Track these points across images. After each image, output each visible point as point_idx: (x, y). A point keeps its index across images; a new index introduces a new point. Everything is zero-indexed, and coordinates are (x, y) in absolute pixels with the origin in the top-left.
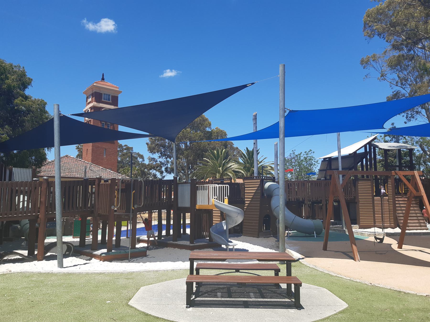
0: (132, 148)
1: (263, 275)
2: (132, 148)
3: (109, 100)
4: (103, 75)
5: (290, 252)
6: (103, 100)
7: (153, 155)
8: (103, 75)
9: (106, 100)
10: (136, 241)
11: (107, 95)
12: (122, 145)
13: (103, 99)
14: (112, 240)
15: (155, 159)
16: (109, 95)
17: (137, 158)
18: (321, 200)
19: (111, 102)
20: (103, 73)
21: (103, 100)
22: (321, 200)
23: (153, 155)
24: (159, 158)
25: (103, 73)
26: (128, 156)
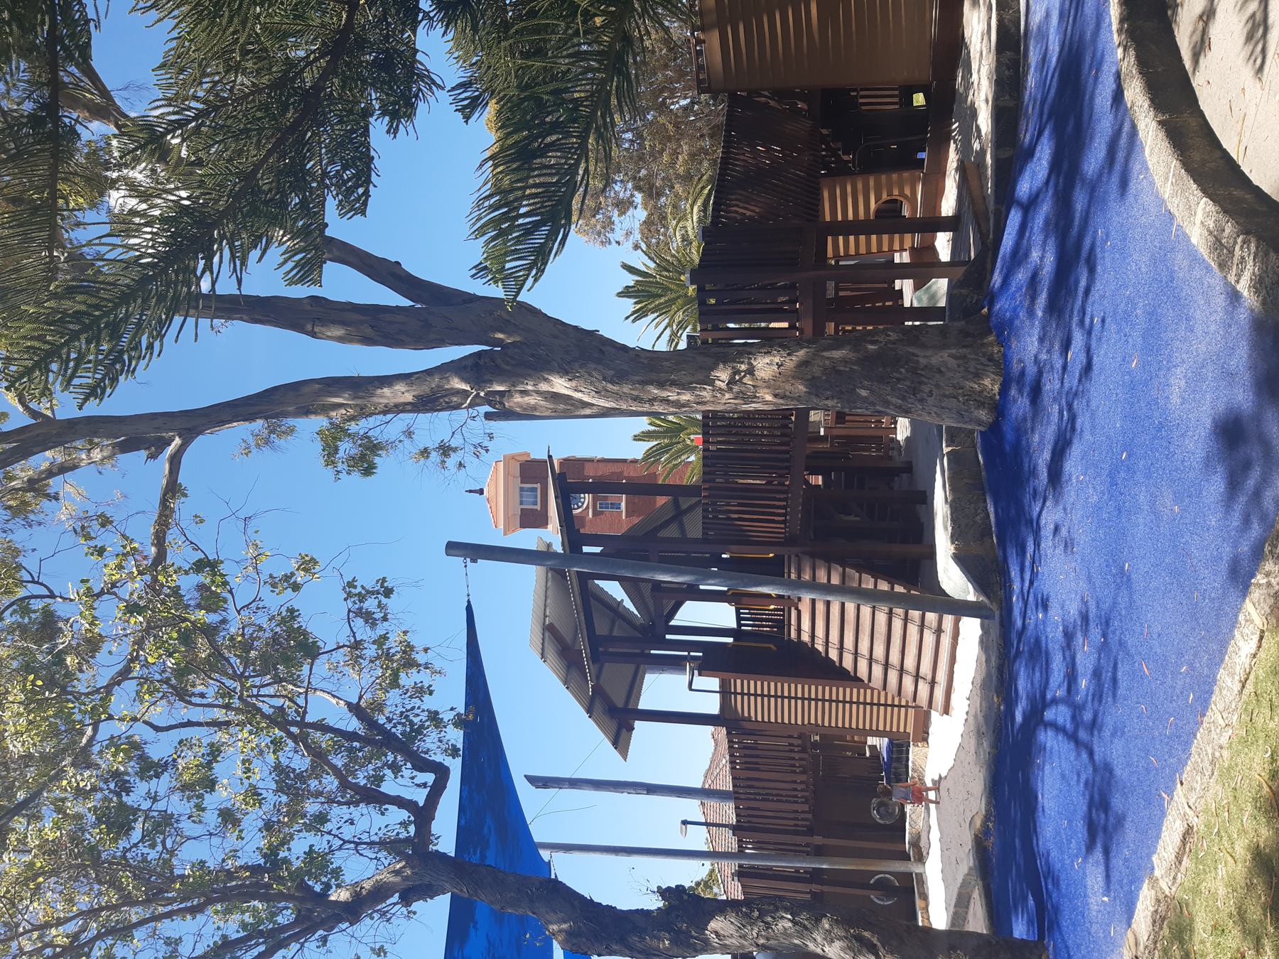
3: (534, 490)
4: (471, 491)
6: (538, 507)
8: (471, 491)
11: (521, 496)
13: (535, 507)
16: (522, 489)
19: (538, 486)
21: (538, 507)
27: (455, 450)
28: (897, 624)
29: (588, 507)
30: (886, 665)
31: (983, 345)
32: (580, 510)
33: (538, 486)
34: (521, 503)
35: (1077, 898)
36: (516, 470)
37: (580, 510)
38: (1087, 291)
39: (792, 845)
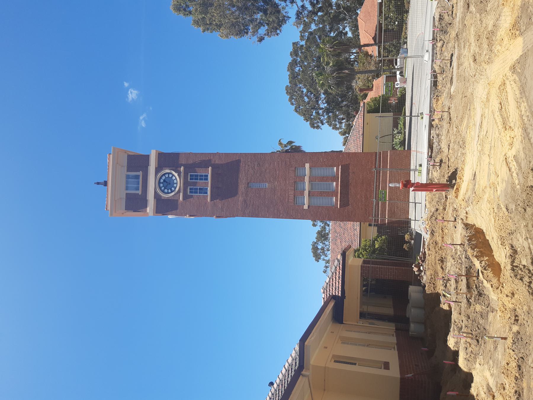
0: (294, 44)
1: (323, 339)
2: (294, 44)
3: (137, 177)
4: (98, 183)
5: (437, 266)
6: (140, 192)
7: (290, 18)
8: (98, 183)
9: (138, 184)
10: (395, 66)
11: (127, 183)
12: (290, 62)
13: (137, 192)
14: (363, 154)
15: (298, 11)
16: (128, 177)
17: (311, 32)
18: (504, 288)
19: (140, 173)
20: (95, 183)
21: (140, 192)
22: (504, 288)
23: (290, 18)
24: (294, 4)
25: (95, 183)
26: (307, 50)
27: (503, 371)
28: (358, 151)
29: (179, 191)
30: (355, 135)
31: (343, 23)
32: (173, 194)
33: (140, 173)
34: (127, 188)
35: (319, 237)
36: (124, 161)
37: (173, 194)
38: (376, 30)
39: (376, 161)
